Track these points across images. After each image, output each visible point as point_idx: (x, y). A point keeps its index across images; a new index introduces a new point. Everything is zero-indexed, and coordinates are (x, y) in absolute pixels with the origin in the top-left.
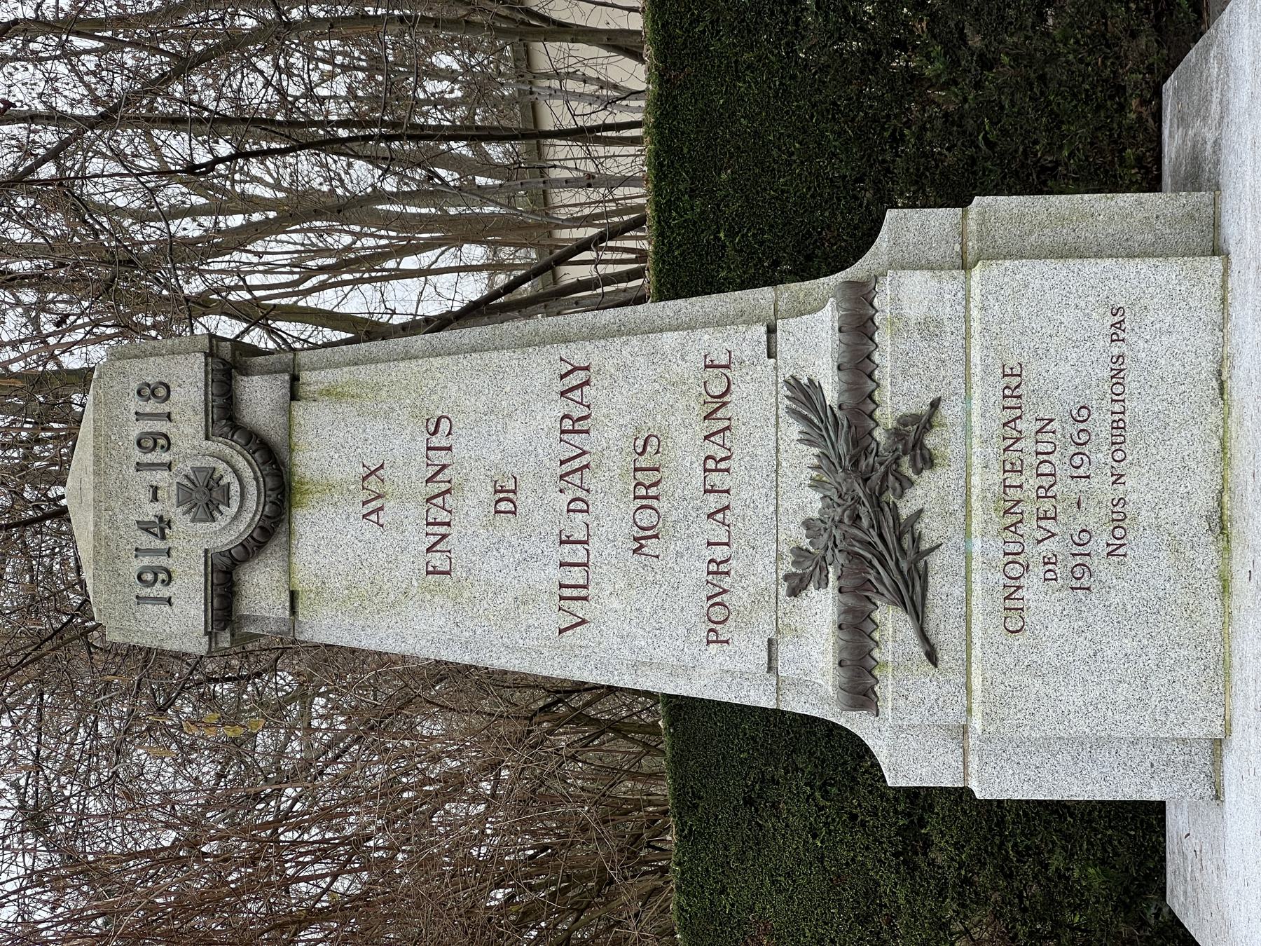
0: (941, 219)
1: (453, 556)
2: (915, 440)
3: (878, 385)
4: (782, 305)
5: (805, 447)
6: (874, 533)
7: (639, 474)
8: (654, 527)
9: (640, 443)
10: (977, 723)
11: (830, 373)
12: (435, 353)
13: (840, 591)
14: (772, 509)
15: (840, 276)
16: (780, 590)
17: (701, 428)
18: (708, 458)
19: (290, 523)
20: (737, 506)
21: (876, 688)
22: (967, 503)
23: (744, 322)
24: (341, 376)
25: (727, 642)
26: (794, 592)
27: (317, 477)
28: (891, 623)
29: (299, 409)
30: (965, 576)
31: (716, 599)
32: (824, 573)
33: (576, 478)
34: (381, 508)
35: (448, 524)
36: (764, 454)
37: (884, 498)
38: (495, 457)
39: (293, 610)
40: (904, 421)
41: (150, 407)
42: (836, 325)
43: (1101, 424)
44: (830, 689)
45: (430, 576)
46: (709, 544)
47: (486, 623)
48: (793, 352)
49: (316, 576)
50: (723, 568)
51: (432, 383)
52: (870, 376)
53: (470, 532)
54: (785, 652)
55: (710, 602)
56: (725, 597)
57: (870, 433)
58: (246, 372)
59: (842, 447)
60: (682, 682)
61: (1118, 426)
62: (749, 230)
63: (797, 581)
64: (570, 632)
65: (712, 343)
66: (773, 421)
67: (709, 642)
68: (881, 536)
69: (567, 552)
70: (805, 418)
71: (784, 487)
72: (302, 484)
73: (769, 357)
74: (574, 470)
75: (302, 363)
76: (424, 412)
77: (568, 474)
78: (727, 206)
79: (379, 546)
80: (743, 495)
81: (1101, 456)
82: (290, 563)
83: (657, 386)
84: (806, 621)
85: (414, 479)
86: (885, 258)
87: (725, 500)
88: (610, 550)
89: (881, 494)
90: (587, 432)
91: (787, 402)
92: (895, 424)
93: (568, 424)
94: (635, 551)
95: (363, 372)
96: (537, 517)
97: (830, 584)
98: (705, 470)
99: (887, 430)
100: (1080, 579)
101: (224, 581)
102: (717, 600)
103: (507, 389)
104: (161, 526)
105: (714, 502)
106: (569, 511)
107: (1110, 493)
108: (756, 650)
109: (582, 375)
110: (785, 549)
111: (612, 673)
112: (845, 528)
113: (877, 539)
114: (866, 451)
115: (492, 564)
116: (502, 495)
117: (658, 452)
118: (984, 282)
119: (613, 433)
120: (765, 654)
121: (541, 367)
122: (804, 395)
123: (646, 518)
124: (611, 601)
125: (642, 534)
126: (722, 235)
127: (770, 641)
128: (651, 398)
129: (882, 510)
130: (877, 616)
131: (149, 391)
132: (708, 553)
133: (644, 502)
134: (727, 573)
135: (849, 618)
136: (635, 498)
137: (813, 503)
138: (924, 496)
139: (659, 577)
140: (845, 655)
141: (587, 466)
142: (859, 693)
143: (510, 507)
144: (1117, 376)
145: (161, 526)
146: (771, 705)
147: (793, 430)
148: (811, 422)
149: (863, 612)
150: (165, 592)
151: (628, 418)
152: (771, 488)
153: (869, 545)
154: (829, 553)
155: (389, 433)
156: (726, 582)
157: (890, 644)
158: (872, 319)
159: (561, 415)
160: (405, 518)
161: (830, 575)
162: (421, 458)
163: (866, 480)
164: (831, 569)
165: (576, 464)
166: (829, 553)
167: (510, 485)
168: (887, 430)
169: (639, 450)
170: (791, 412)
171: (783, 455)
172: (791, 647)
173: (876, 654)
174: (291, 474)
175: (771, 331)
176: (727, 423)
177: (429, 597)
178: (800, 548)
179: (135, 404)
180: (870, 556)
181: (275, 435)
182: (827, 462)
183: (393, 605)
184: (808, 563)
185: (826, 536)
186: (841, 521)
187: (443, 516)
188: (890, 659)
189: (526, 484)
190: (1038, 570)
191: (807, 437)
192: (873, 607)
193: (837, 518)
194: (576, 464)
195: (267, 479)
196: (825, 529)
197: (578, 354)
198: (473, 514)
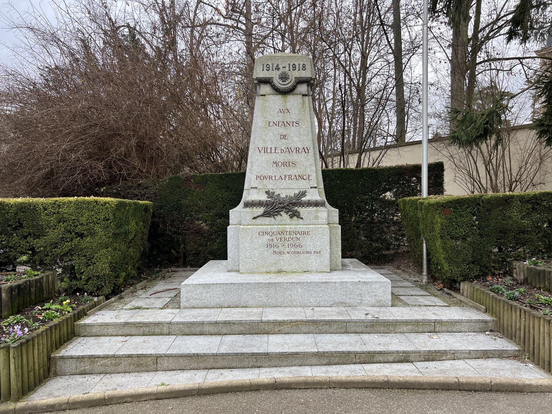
26: (266, 192)
29: (301, 96)
31: (265, 177)
33: (287, 150)
39: (261, 95)
54: (255, 190)
59: (294, 201)
74: (289, 150)
87: (284, 179)
110: (274, 190)
114: (293, 205)
115: (271, 134)
122: (304, 194)
124: (264, 157)
130: (262, 208)
132: (273, 176)
137: (283, 196)
153: (275, 206)
160: (280, 118)
162: (291, 120)
175: (315, 188)
181: (295, 91)
187: (280, 125)
189: (286, 141)
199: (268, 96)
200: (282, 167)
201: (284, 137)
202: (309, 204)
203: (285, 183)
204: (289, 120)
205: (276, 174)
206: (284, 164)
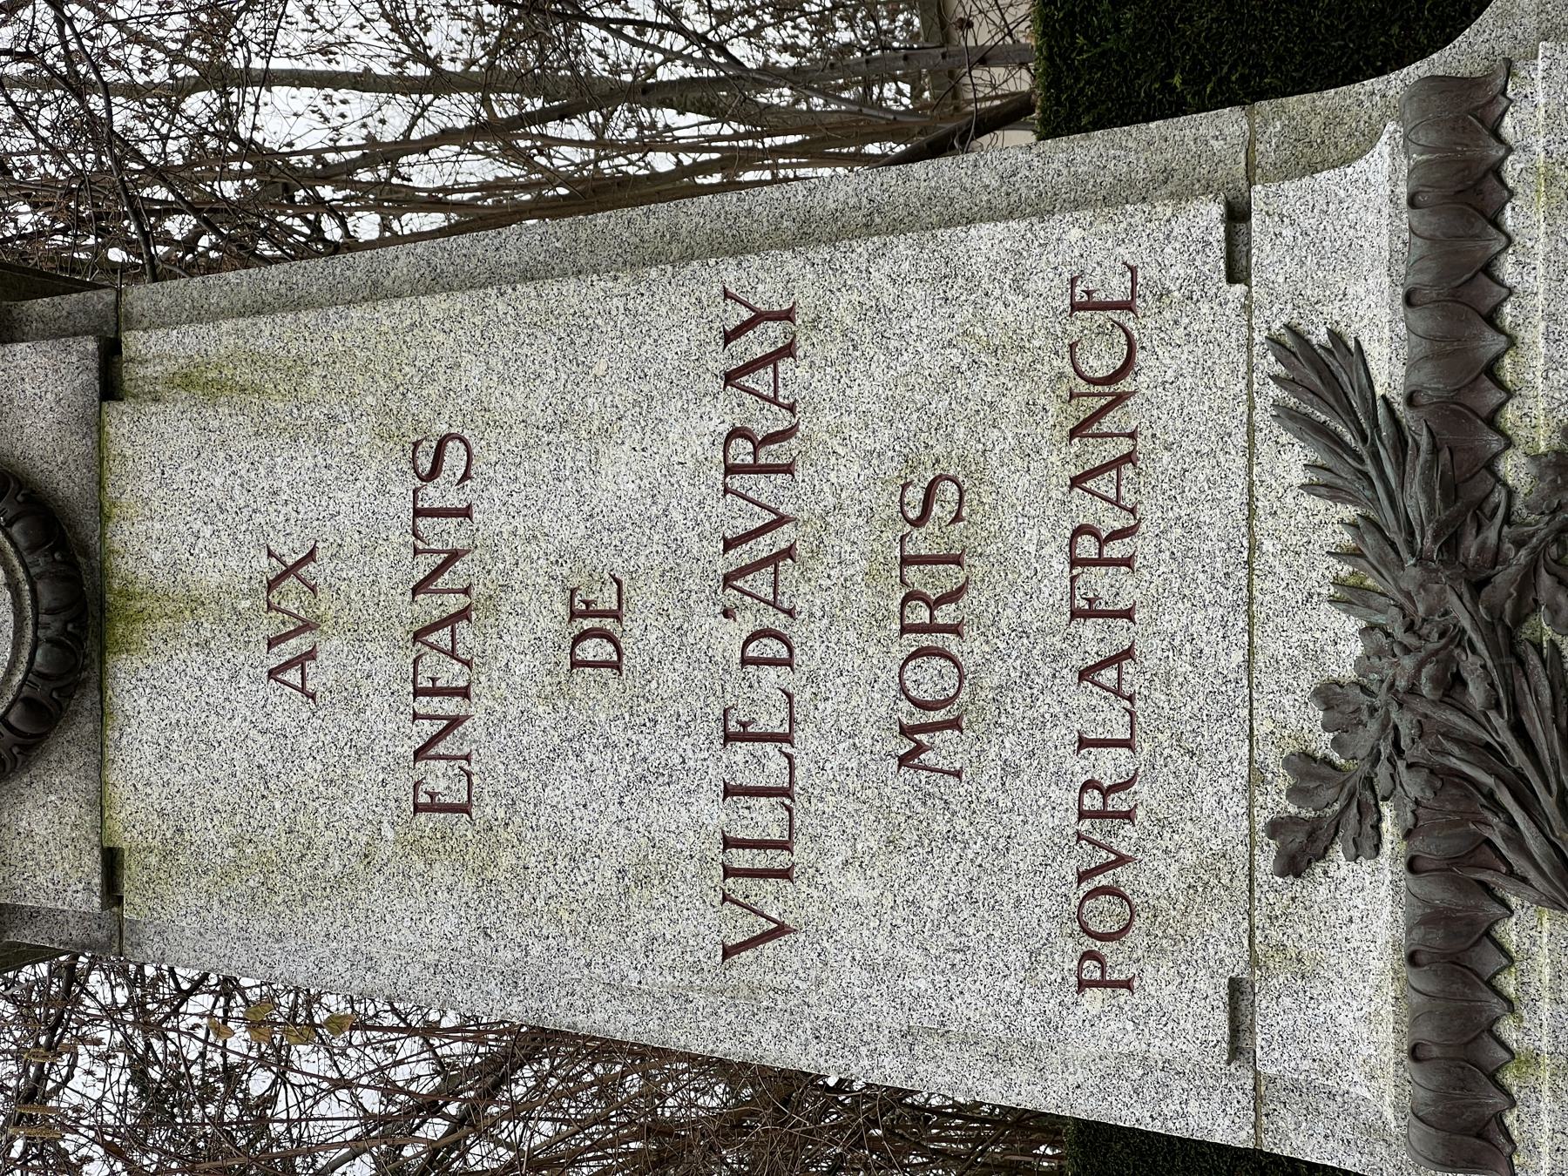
1: (475, 768)
3: (1512, 342)
4: (1267, 151)
5: (1321, 504)
6: (1499, 722)
7: (912, 573)
8: (949, 701)
9: (915, 495)
11: (1384, 315)
13: (1412, 866)
14: (1238, 657)
15: (1417, 70)
16: (1259, 859)
17: (1063, 459)
18: (1079, 531)
19: (101, 690)
20: (1152, 651)
21: (1510, 1119)
23: (1171, 195)
24: (214, 341)
25: (1127, 984)
26: (1294, 865)
27: (163, 581)
29: (120, 420)
31: (1101, 878)
32: (1369, 822)
33: (760, 583)
34: (311, 655)
35: (464, 693)
36: (1219, 522)
37: (1526, 632)
38: (571, 532)
39: (112, 891)
42: (1403, 190)
44: (1389, 1114)
45: (422, 817)
46: (1083, 743)
47: (552, 930)
48: (1291, 266)
49: (162, 813)
50: (1117, 802)
51: (424, 357)
52: (1491, 318)
53: (513, 711)
54: (1273, 1014)
55: (1086, 887)
56: (1123, 875)
57: (1490, 466)
59: (1415, 501)
60: (1021, 1076)
62: (1233, 68)
63: (1301, 837)
64: (748, 955)
65: (1085, 246)
66: (1240, 438)
67: (1082, 985)
68: (1519, 730)
69: (741, 762)
70: (1321, 430)
72: (130, 597)
73: (1232, 278)
74: (757, 562)
75: (136, 311)
76: (408, 425)
77: (742, 572)
78: (1188, 20)
79: (306, 743)
80: (1168, 623)
82: (102, 783)
83: (955, 356)
84: (1325, 937)
85: (384, 583)
86: (1531, 22)
87: (1121, 635)
88: (843, 756)
89: (1520, 619)
90: (788, 469)
91: (1274, 390)
92: (1556, 441)
93: (742, 451)
94: (903, 761)
95: (269, 333)
96: (671, 676)
97: (1386, 848)
98: (1074, 562)
99: (1535, 457)
102: (1102, 880)
103: (600, 369)
105: (1094, 639)
106: (745, 661)
108: (1199, 1007)
109: (774, 332)
110: (1271, 757)
111: (854, 1050)
112: (1423, 707)
113: (1507, 738)
114: (1480, 513)
115: (564, 788)
116: (588, 624)
117: (957, 518)
119: (850, 472)
120: (1222, 1017)
122: (1318, 372)
123: (930, 679)
124: (842, 882)
125: (921, 717)
126: (1177, 80)
127: (1236, 989)
128: (942, 387)
129: (1522, 662)
130: (1510, 933)
132: (1080, 767)
133: (926, 640)
134: (1129, 816)
135: (1437, 938)
136: (904, 629)
137: (1343, 644)
139: (961, 824)
140: (1426, 1032)
141: (788, 553)
142: (1464, 1131)
143: (607, 651)
146: (1241, 1138)
147: (1291, 460)
148: (1337, 440)
149: (1472, 923)
151: (885, 435)
152: (1235, 607)
153: (1488, 753)
154: (1383, 770)
155: (328, 475)
156: (1126, 838)
157: (1545, 1007)
158: (1496, 170)
159: (725, 428)
160: (367, 670)
161: (1386, 826)
162: (399, 537)
163: (1478, 586)
164: (1387, 810)
165: (763, 547)
166: (1383, 770)
167: (606, 599)
168: (1535, 457)
169: (913, 514)
170: (1286, 415)
171: (1265, 524)
172: (1287, 1001)
173: (1508, 1030)
174: (103, 573)
175: (1237, 215)
176: (1125, 446)
177: (420, 866)
178: (1307, 756)
180: (1489, 781)
181: (67, 482)
182: (1375, 541)
183: (337, 884)
184: (1329, 794)
185: (1373, 726)
186: (1413, 690)
187: (451, 674)
188: (1545, 1044)
189: (645, 597)
191: (1325, 477)
192: (1497, 910)
193: (1402, 683)
194: (763, 547)
195: (40, 587)
196: (1373, 710)
197: (766, 280)
198: (521, 669)
199: (120, 817)
200: (970, 648)
201: (594, 623)
202: (1458, 285)
203: (1178, 614)
204: (394, 565)
205: (1062, 735)
206: (930, 607)
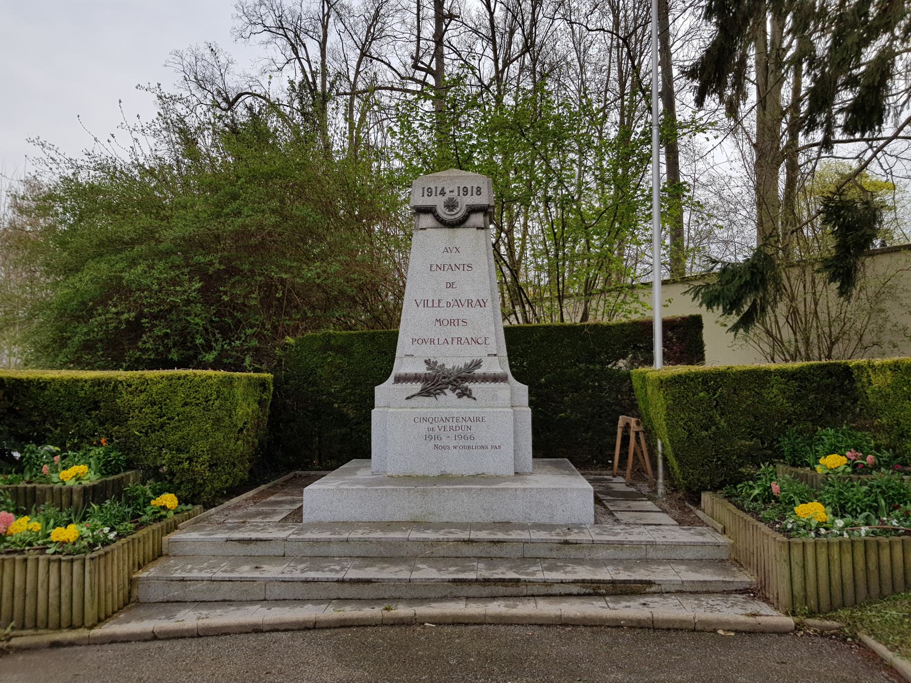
0: (525, 400)
2: (465, 393)
10: (390, 410)
12: (490, 266)
20: (448, 346)
22: (448, 407)
26: (426, 361)
28: (418, 387)
30: (428, 406)
40: (470, 390)
41: (475, 190)
43: (469, 443)
58: (485, 215)
61: (469, 447)
65: (492, 340)
69: (436, 302)
71: (453, 359)
74: (459, 303)
81: (462, 443)
100: (428, 438)
101: (429, 210)
104: (443, 193)
105: (450, 340)
107: (451, 446)
118: (508, 412)
121: (485, 294)
122: (478, 364)
123: (445, 322)
131: (479, 190)
132: (436, 339)
138: (450, 396)
144: (482, 447)
145: (443, 193)
147: (469, 362)
150: (425, 195)
156: (428, 344)
160: (446, 259)
175: (495, 355)
179: (475, 186)
181: (467, 224)
182: (460, 371)
190: (431, 426)
203: (454, 348)
